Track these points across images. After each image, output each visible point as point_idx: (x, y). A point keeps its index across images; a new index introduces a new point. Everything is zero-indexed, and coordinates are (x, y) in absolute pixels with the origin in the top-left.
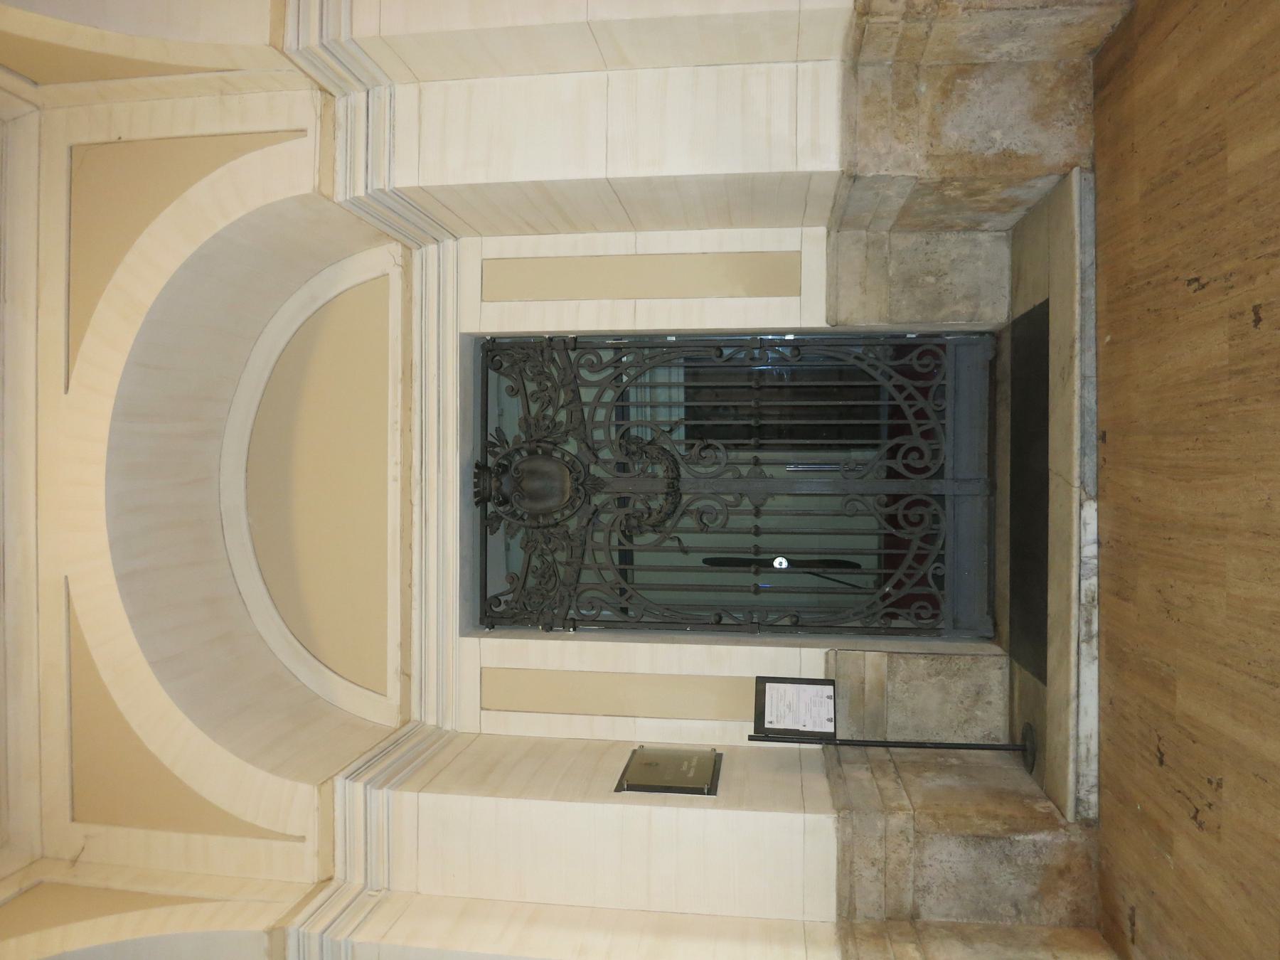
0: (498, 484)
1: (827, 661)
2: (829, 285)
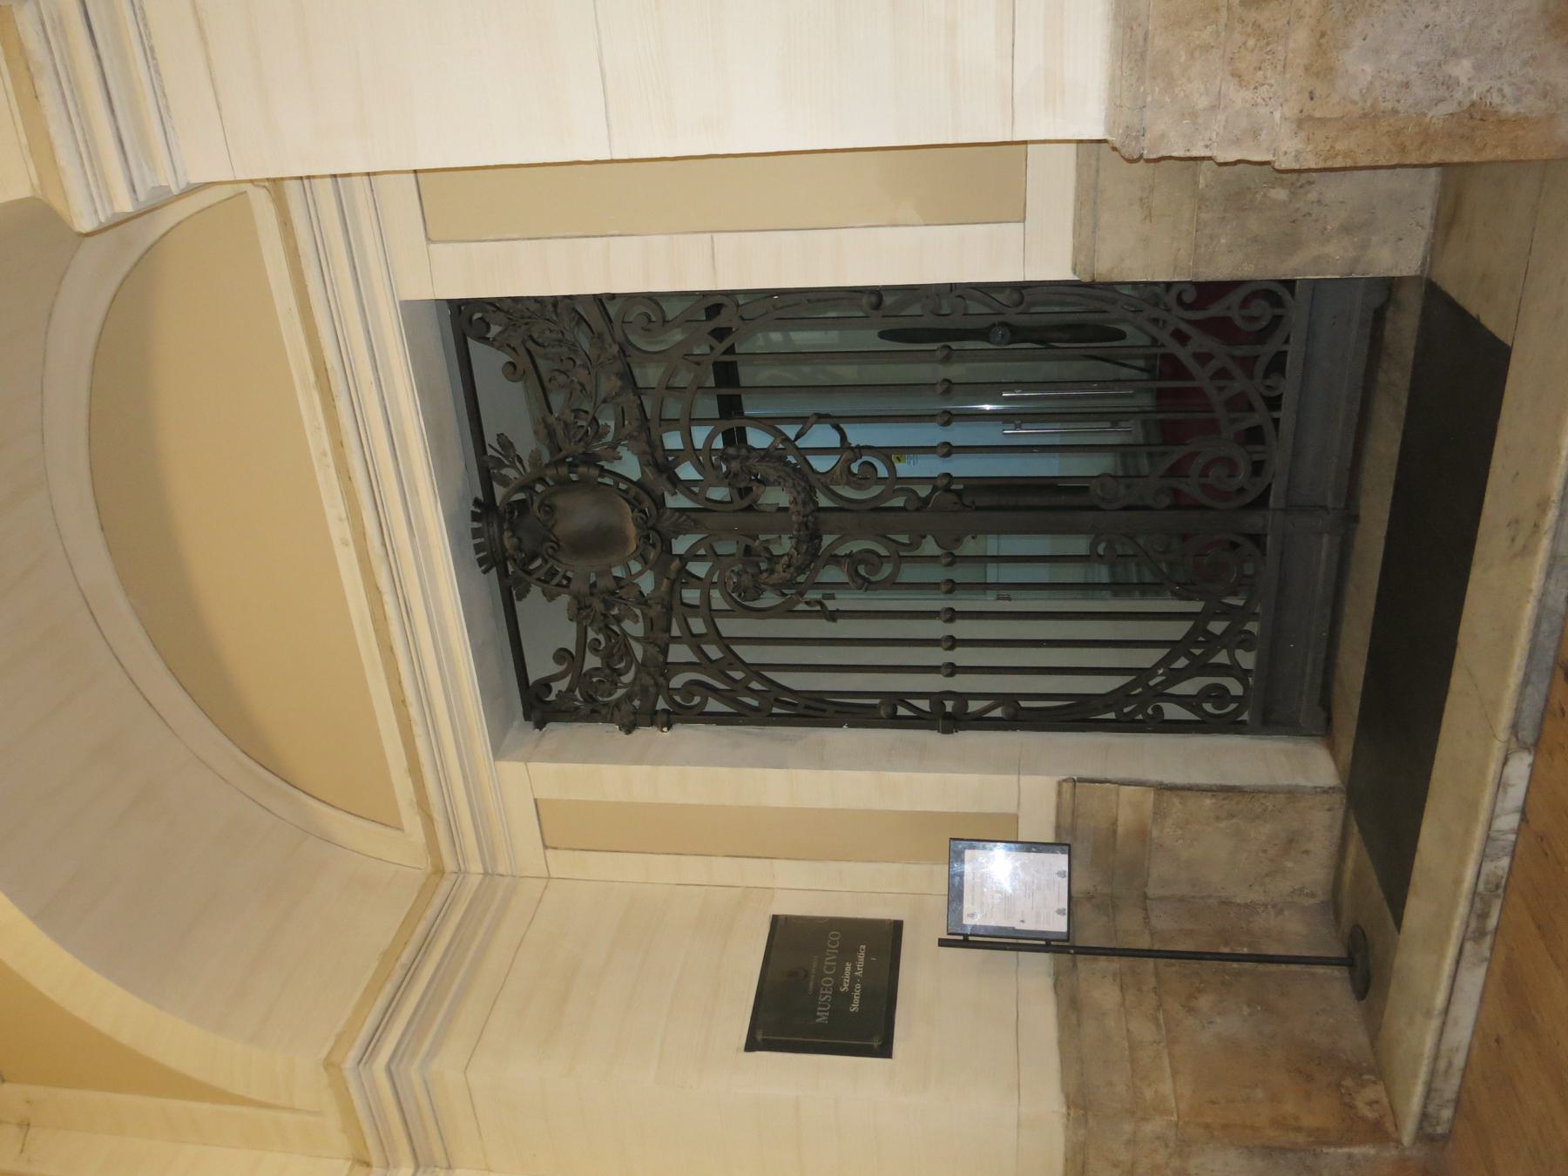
0: (511, 533)
1: (1059, 794)
2: (1080, 202)
